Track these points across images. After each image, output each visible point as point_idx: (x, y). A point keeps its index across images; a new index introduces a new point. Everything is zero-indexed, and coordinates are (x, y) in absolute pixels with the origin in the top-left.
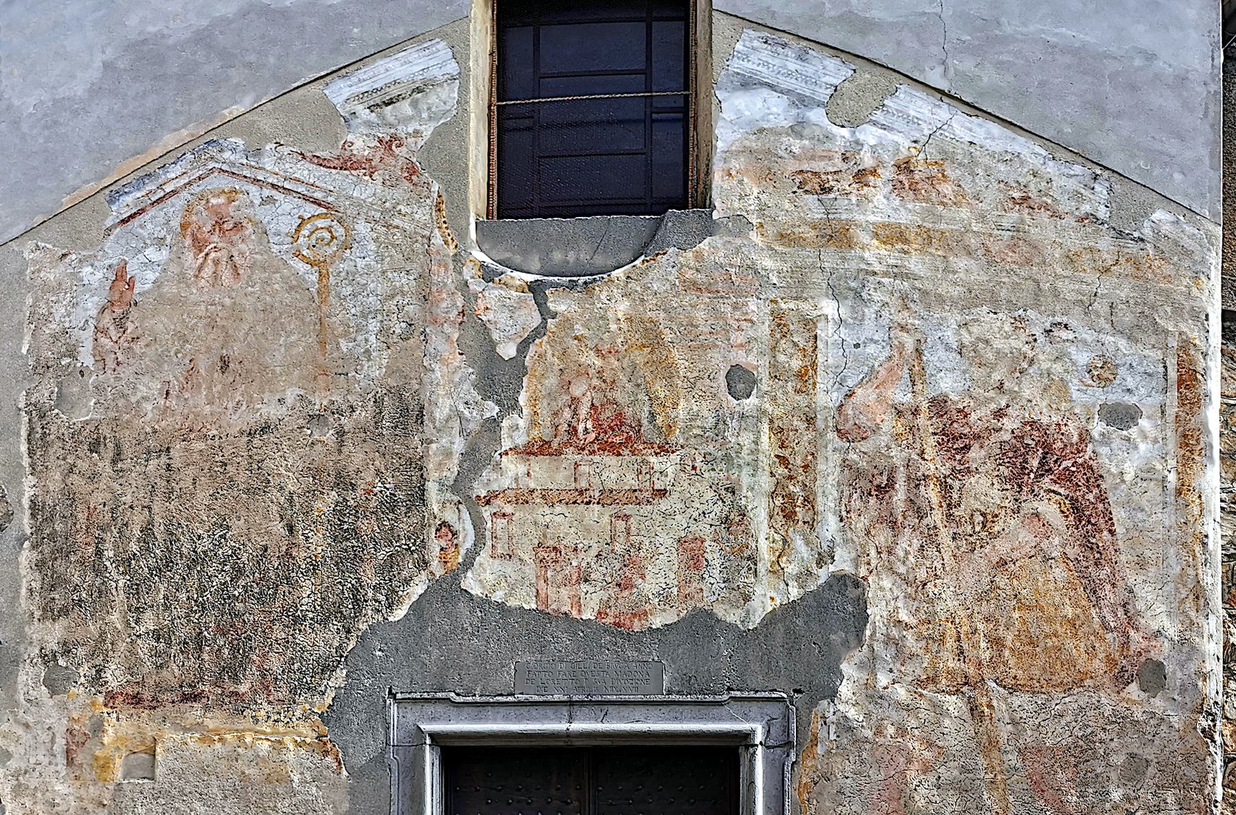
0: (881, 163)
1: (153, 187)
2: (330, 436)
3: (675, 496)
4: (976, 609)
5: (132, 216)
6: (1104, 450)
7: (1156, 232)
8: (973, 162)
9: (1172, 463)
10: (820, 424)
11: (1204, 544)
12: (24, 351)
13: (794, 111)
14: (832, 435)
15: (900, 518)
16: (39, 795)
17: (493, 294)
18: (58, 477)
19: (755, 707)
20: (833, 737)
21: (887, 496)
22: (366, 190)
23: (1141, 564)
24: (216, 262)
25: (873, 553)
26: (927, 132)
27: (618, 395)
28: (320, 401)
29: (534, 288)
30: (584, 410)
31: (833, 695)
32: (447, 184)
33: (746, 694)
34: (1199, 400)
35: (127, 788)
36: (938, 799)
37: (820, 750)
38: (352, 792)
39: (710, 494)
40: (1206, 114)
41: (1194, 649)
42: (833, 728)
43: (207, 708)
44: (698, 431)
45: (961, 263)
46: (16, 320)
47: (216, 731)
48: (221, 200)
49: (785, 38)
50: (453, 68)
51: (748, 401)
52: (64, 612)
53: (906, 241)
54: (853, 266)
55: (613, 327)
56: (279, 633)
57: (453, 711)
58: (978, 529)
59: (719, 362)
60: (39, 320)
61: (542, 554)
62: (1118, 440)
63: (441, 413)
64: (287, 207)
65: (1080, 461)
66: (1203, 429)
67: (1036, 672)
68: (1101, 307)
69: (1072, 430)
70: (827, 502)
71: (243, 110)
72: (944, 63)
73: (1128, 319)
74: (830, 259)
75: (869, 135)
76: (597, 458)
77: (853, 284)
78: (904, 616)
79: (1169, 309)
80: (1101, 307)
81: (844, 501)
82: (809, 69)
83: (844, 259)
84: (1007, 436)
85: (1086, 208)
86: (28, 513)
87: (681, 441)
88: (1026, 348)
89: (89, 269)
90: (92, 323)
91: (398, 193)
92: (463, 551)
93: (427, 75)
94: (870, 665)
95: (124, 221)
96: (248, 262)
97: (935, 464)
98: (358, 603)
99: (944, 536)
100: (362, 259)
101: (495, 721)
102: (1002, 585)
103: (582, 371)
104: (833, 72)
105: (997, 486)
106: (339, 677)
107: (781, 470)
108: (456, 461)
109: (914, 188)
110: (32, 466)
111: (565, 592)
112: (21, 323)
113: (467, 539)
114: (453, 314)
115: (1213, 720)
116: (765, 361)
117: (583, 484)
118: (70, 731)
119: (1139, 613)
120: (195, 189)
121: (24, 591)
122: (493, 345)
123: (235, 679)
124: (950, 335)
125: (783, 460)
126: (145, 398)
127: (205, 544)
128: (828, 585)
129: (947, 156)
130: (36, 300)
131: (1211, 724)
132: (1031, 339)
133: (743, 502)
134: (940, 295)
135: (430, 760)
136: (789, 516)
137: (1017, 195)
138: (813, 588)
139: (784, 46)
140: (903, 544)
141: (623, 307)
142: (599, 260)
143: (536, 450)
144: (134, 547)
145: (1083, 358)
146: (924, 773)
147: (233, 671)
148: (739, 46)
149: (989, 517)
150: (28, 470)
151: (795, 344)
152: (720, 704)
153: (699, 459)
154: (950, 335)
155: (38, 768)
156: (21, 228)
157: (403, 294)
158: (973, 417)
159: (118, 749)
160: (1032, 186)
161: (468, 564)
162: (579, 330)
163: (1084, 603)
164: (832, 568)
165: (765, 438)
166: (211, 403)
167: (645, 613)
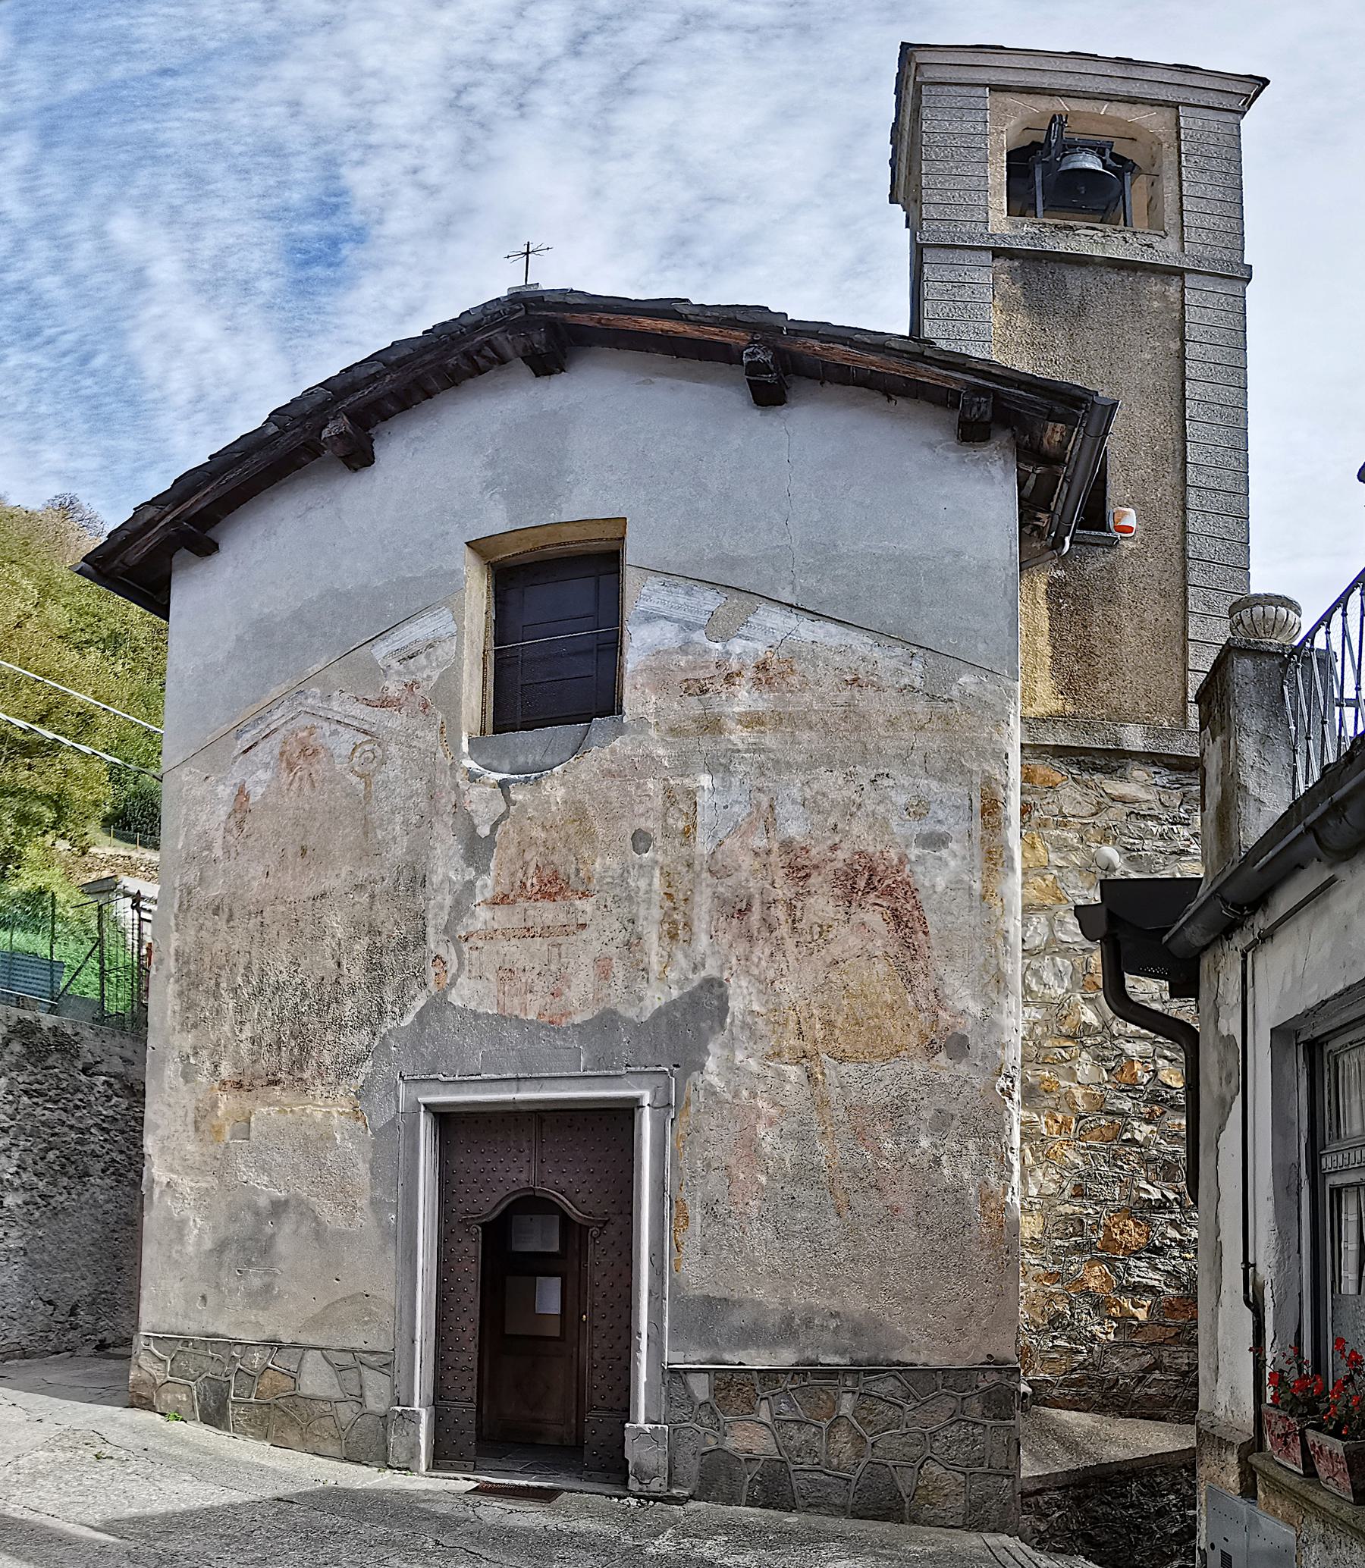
0: (744, 666)
1: (262, 726)
2: (365, 899)
3: (592, 928)
4: (814, 999)
5: (250, 748)
6: (919, 869)
7: (963, 695)
8: (815, 657)
9: (978, 874)
10: (697, 867)
11: (1005, 939)
12: (180, 847)
13: (682, 635)
14: (705, 875)
15: (756, 934)
16: (176, 1153)
17: (475, 792)
18: (193, 933)
19: (645, 1078)
20: (702, 1099)
21: (745, 918)
22: (394, 721)
23: (950, 957)
24: (301, 779)
25: (734, 961)
26: (780, 639)
27: (555, 858)
28: (362, 875)
29: (503, 785)
30: (531, 870)
31: (701, 1067)
32: (446, 712)
33: (638, 1069)
34: (1000, 823)
35: (232, 1146)
36: (781, 1146)
37: (692, 1109)
38: (374, 1145)
39: (617, 925)
40: (1005, 594)
41: (994, 1024)
42: (702, 1092)
43: (283, 1089)
44: (609, 880)
45: (805, 736)
46: (175, 825)
47: (288, 1105)
48: (305, 734)
49: (677, 580)
50: (453, 627)
51: (646, 855)
52: (195, 1026)
53: (763, 724)
54: (723, 746)
55: (554, 808)
56: (330, 1037)
57: (441, 1087)
58: (816, 937)
59: (626, 829)
60: (191, 825)
61: (501, 974)
62: (931, 860)
63: (436, 879)
64: (346, 737)
65: (899, 879)
66: (1005, 846)
67: (860, 1046)
68: (917, 757)
69: (893, 855)
70: (701, 927)
71: (320, 668)
72: (792, 583)
73: (940, 764)
74: (706, 744)
75: (737, 646)
76: (539, 904)
77: (723, 761)
78: (756, 1007)
79: (973, 753)
80: (917, 757)
81: (714, 923)
82: (694, 601)
83: (716, 742)
84: (840, 865)
85: (905, 681)
86: (173, 958)
87: (597, 888)
88: (855, 796)
89: (222, 787)
90: (222, 825)
91: (415, 722)
92: (450, 975)
93: (437, 634)
94: (731, 1045)
95: (245, 752)
96: (320, 778)
97: (783, 891)
98: (381, 1013)
99: (790, 944)
100: (392, 771)
101: (468, 1093)
102: (834, 980)
103: (532, 841)
104: (710, 601)
105: (831, 903)
106: (367, 1067)
107: (668, 904)
108: (446, 912)
109: (769, 681)
110: (177, 925)
111: (516, 1001)
112: (178, 827)
113: (453, 968)
114: (448, 809)
115: (1012, 1082)
116: (659, 825)
117: (530, 924)
118: (197, 1108)
119: (946, 996)
120: (289, 726)
121: (169, 1012)
122: (474, 828)
123: (302, 1070)
124: (795, 793)
125: (669, 896)
126: (254, 878)
127: (284, 977)
128: (701, 987)
129: (795, 654)
130: (189, 810)
131: (1010, 1085)
132: (859, 789)
133: (640, 928)
134: (788, 762)
135: (425, 1123)
136: (673, 936)
137: (849, 677)
138: (689, 989)
139: (675, 586)
140: (757, 952)
141: (560, 793)
142: (548, 760)
143: (500, 900)
144: (239, 980)
145: (901, 799)
146: (770, 1126)
147: (298, 1064)
148: (644, 591)
149: (825, 928)
150: (174, 928)
151: (680, 810)
152: (620, 1076)
153: (610, 899)
154: (795, 793)
155: (176, 1134)
156: (180, 759)
157: (418, 795)
158: (813, 852)
159: (227, 1119)
160: (861, 669)
161: (452, 984)
162: (531, 812)
163: (900, 990)
164: (703, 974)
165: (656, 881)
166: (294, 879)
167: (570, 1013)
